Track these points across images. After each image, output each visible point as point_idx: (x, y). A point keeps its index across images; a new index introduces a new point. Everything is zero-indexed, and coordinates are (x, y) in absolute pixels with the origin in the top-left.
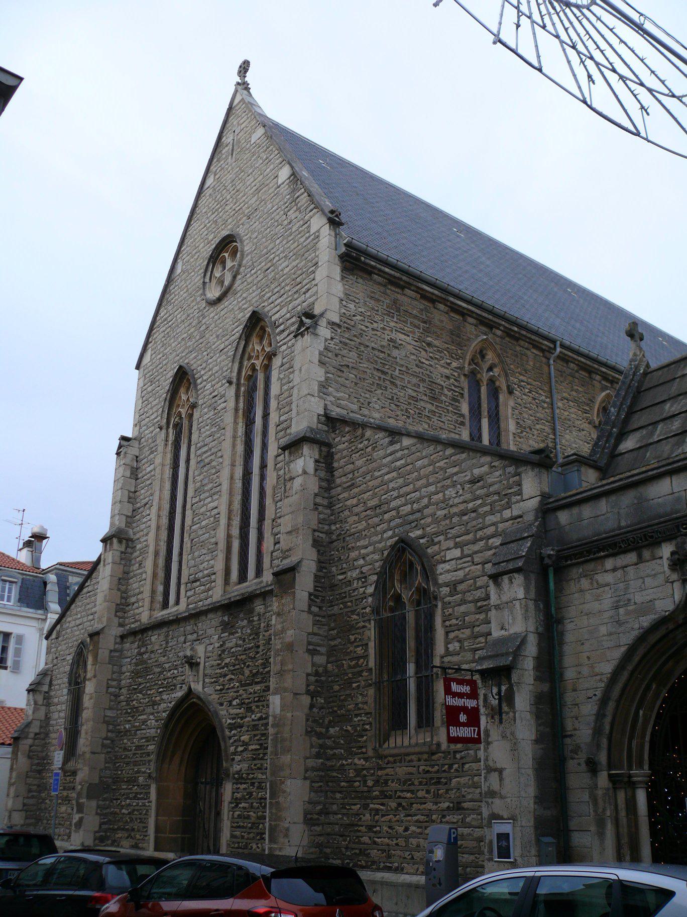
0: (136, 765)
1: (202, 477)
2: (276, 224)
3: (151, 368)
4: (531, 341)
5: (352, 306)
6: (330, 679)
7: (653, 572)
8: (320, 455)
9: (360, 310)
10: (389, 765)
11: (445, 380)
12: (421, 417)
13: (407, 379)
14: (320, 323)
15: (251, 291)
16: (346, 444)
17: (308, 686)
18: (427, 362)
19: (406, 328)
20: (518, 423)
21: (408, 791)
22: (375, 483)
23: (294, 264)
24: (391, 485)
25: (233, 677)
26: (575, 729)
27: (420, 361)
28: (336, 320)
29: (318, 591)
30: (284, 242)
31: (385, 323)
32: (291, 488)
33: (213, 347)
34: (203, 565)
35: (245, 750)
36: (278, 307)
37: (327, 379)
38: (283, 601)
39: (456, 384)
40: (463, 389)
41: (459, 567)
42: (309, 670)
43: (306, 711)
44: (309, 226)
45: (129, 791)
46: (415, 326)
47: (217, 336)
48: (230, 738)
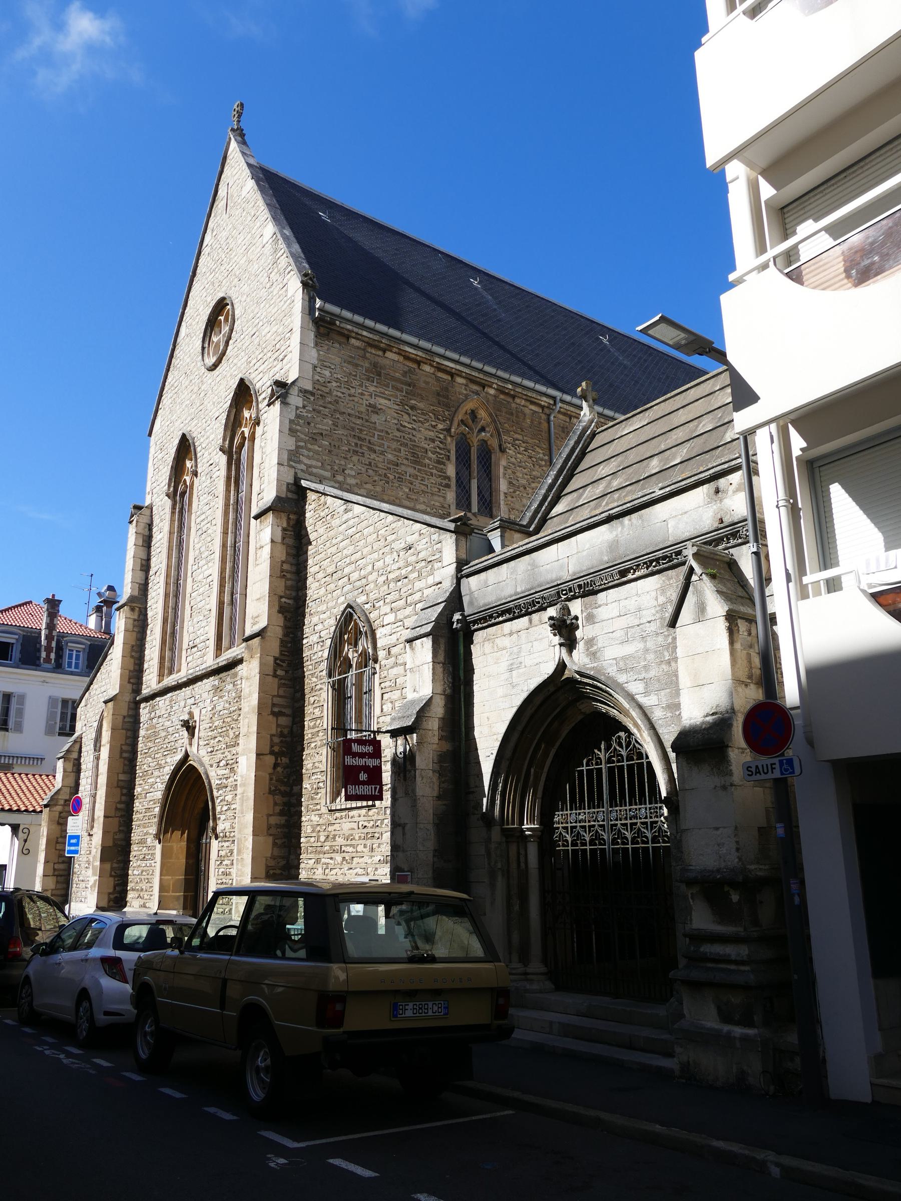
0: (145, 827)
1: (200, 545)
2: (261, 286)
3: (161, 435)
4: (529, 398)
5: (327, 373)
6: (295, 740)
7: (540, 636)
8: (288, 523)
9: (335, 375)
10: (338, 821)
11: (430, 443)
12: (402, 482)
13: (386, 444)
14: (291, 391)
15: (240, 357)
16: (312, 512)
17: (272, 746)
18: (410, 426)
19: (386, 392)
20: (510, 483)
21: (350, 845)
22: (334, 550)
23: (274, 329)
24: (345, 552)
25: (221, 739)
26: (476, 787)
27: (401, 425)
28: (309, 387)
29: (284, 655)
30: (267, 306)
31: (364, 388)
32: (261, 556)
33: (210, 414)
34: (199, 632)
35: (229, 809)
36: (261, 375)
37: (298, 447)
38: (251, 666)
39: (441, 446)
40: (449, 452)
41: (393, 631)
42: (274, 732)
43: (271, 770)
44: (287, 290)
45: (140, 853)
46: (397, 389)
47: (214, 403)
48: (217, 797)
